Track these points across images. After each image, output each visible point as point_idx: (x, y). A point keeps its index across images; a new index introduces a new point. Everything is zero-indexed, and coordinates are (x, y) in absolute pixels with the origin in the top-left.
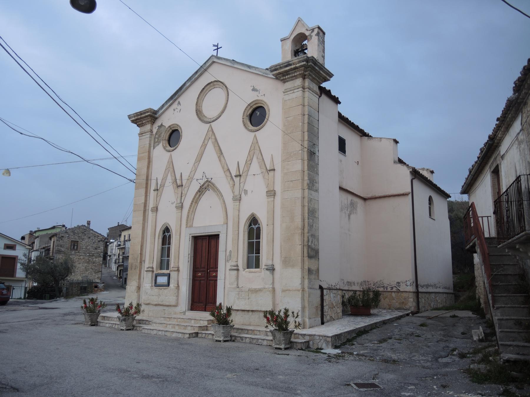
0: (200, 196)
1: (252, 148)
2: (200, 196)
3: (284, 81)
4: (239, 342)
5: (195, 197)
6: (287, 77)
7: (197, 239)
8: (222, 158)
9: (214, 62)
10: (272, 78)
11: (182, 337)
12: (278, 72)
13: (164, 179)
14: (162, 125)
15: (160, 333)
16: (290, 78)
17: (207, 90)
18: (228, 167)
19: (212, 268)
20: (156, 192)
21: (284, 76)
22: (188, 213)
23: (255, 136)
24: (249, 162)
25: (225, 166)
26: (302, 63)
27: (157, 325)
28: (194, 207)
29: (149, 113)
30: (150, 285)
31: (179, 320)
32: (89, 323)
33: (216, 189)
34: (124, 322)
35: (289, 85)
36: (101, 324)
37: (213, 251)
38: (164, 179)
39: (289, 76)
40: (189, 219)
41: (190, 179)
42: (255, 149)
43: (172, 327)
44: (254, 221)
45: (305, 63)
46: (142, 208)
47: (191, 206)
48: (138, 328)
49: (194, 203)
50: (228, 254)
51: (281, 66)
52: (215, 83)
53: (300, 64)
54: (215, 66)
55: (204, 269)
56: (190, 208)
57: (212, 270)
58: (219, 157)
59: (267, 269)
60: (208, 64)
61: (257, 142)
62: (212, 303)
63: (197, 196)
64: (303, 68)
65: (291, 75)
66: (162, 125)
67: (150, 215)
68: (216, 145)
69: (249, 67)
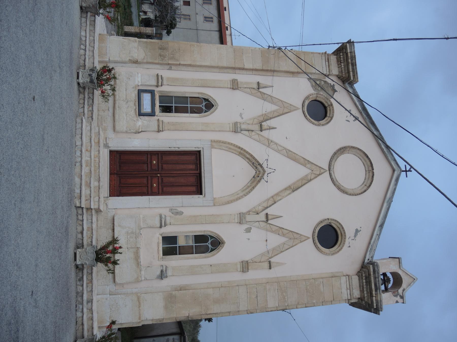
0: (248, 158)
1: (296, 236)
2: (248, 158)
3: (359, 274)
4: (77, 276)
5: (247, 152)
6: (364, 281)
7: (195, 157)
8: (288, 192)
9: (394, 171)
10: (365, 257)
11: (76, 195)
12: (372, 273)
13: (270, 99)
14: (335, 91)
15: (78, 153)
16: (363, 284)
17: (366, 161)
18: (278, 201)
19: (162, 179)
20: (255, 86)
21: (366, 278)
22: (229, 143)
23: (297, 109)
24: (280, 231)
25: (280, 198)
26: (375, 305)
27: (89, 134)
28: (235, 150)
29: (352, 78)
30: (139, 84)
31: (97, 159)
32: (84, 5)
33: (255, 183)
34: (88, 80)
35: (355, 280)
36: (84, 20)
37: (184, 189)
38: (270, 99)
39: (365, 284)
40: (221, 144)
41: (269, 143)
42: (294, 238)
43: (87, 161)
44: (209, 105)
45: (375, 307)
46: (237, 66)
47: (237, 146)
48: (82, 96)
49: (239, 150)
50: (180, 209)
51: (377, 279)
52: (371, 174)
53: (375, 301)
54: (390, 171)
55: (160, 169)
56: (234, 145)
57: (160, 180)
58: (290, 187)
59: (162, 271)
60: (393, 163)
61: (301, 242)
62: (120, 183)
63: (248, 156)
64: (370, 303)
65: (365, 286)
66: (335, 91)
67: (227, 77)
68: (304, 182)
69: (382, 226)
